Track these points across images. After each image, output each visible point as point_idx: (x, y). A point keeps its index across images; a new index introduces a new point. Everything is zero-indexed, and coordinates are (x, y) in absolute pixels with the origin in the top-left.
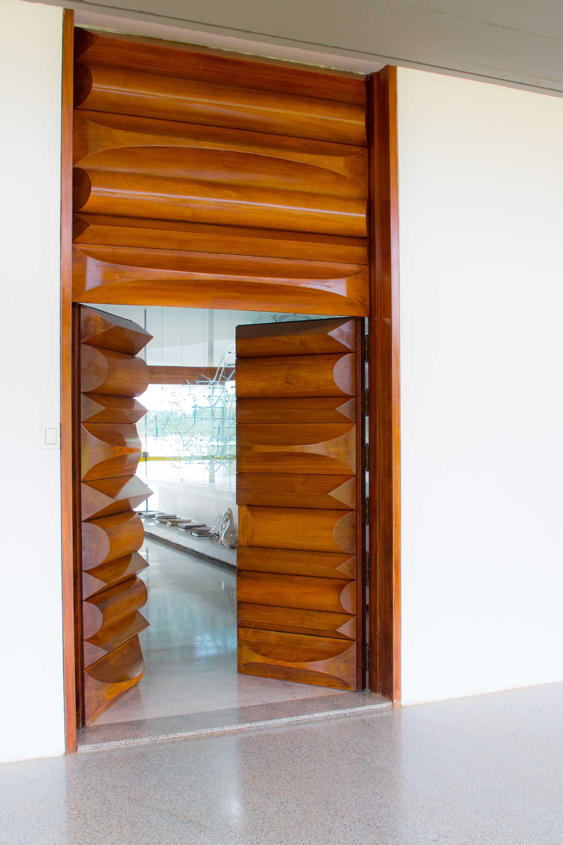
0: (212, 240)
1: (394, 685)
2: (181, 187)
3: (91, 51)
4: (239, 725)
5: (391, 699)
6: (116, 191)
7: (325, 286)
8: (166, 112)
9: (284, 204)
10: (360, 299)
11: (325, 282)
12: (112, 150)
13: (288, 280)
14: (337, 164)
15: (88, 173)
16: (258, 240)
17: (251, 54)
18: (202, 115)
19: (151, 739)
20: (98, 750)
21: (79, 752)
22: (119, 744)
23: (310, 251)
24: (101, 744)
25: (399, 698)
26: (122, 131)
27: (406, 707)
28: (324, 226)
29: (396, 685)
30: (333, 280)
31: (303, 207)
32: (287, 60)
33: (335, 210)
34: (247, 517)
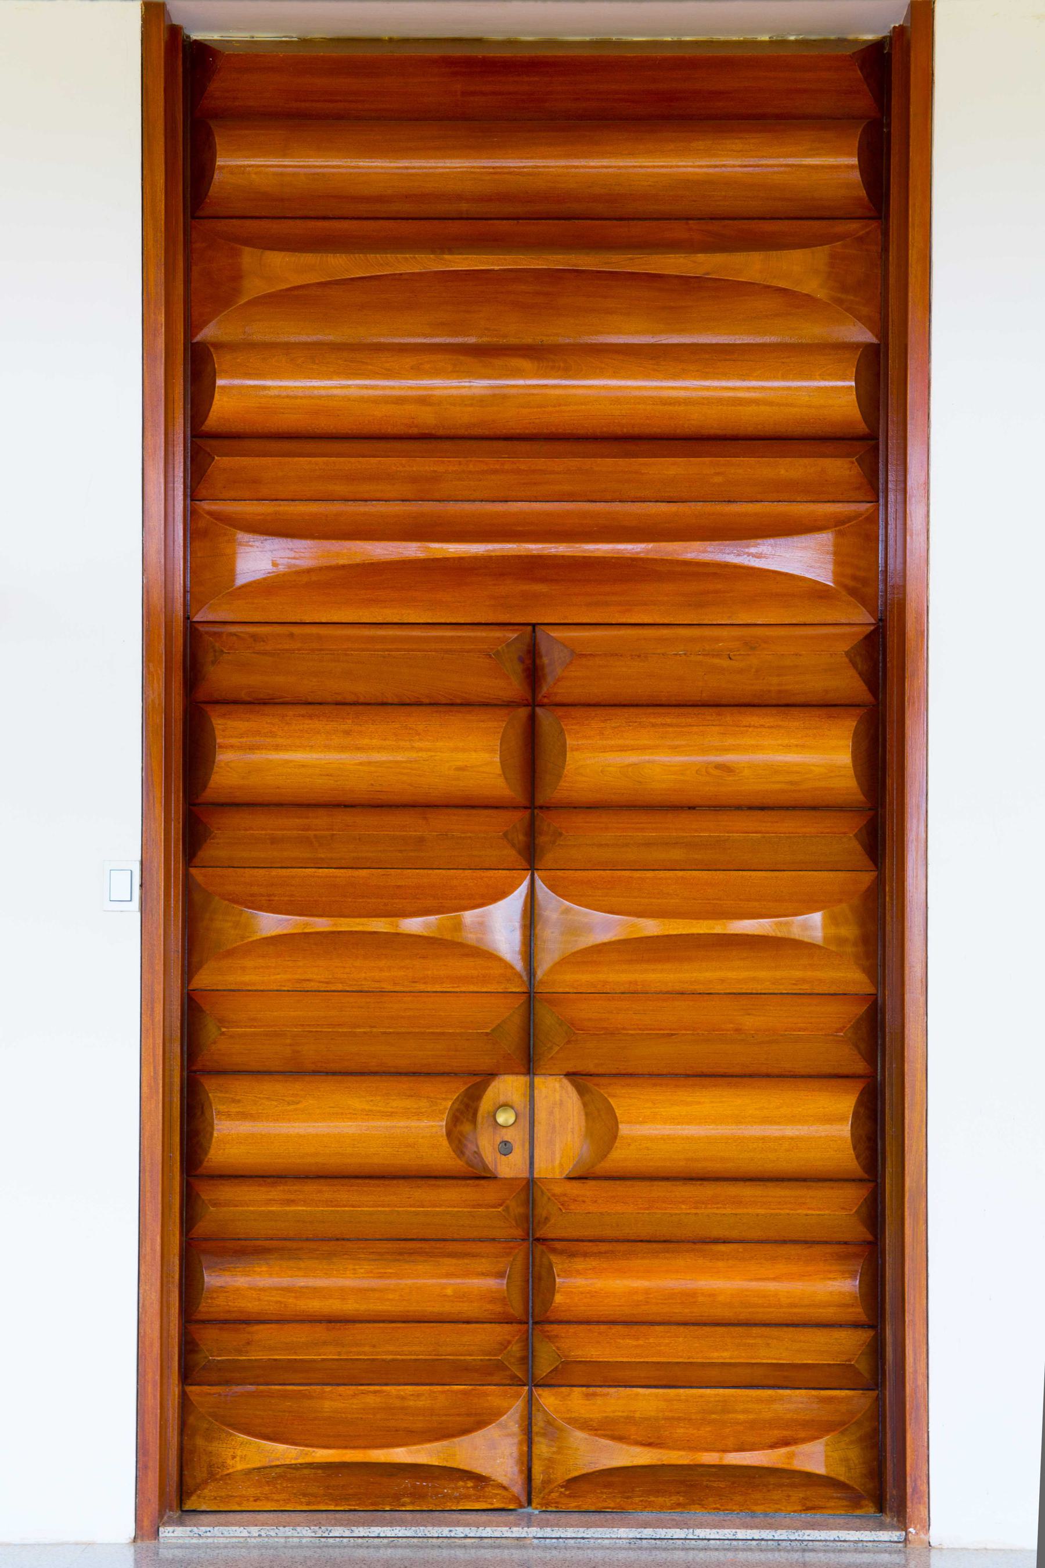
0: (483, 472)
1: (909, 1490)
2: (409, 361)
3: (218, 87)
4: (514, 1529)
5: (901, 1520)
6: (269, 383)
7: (749, 554)
8: (380, 199)
9: (647, 376)
10: (851, 583)
11: (748, 547)
12: (265, 296)
13: (651, 545)
14: (800, 268)
15: (212, 350)
16: (588, 463)
17: (587, 39)
18: (460, 197)
19: (315, 1532)
20: (201, 1541)
21: (161, 1540)
22: (245, 1534)
23: (718, 479)
24: (208, 1529)
25: (927, 1526)
26: (283, 253)
27: (941, 1549)
28: (749, 418)
29: (915, 1490)
30: (771, 541)
31: (695, 378)
32: (675, 39)
33: (775, 378)
34: (561, 1103)
